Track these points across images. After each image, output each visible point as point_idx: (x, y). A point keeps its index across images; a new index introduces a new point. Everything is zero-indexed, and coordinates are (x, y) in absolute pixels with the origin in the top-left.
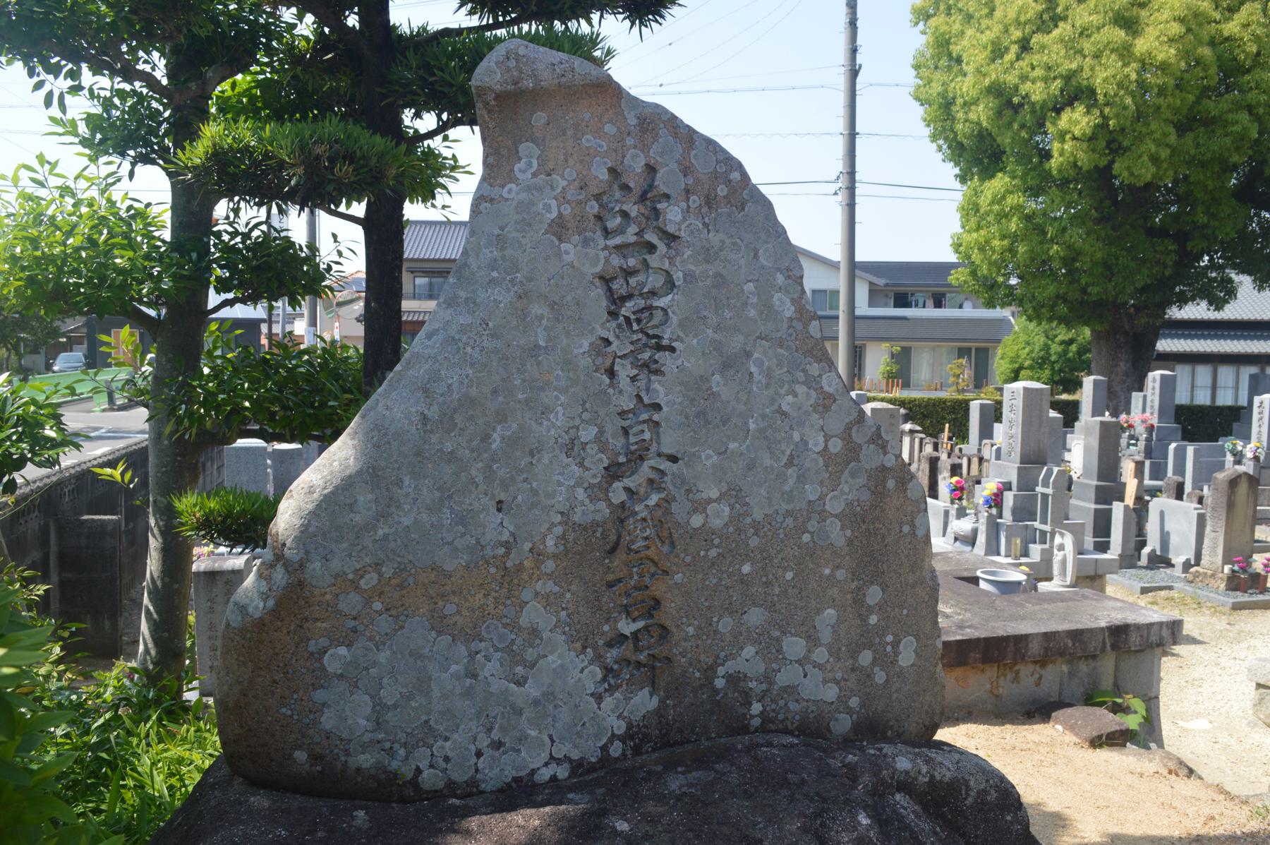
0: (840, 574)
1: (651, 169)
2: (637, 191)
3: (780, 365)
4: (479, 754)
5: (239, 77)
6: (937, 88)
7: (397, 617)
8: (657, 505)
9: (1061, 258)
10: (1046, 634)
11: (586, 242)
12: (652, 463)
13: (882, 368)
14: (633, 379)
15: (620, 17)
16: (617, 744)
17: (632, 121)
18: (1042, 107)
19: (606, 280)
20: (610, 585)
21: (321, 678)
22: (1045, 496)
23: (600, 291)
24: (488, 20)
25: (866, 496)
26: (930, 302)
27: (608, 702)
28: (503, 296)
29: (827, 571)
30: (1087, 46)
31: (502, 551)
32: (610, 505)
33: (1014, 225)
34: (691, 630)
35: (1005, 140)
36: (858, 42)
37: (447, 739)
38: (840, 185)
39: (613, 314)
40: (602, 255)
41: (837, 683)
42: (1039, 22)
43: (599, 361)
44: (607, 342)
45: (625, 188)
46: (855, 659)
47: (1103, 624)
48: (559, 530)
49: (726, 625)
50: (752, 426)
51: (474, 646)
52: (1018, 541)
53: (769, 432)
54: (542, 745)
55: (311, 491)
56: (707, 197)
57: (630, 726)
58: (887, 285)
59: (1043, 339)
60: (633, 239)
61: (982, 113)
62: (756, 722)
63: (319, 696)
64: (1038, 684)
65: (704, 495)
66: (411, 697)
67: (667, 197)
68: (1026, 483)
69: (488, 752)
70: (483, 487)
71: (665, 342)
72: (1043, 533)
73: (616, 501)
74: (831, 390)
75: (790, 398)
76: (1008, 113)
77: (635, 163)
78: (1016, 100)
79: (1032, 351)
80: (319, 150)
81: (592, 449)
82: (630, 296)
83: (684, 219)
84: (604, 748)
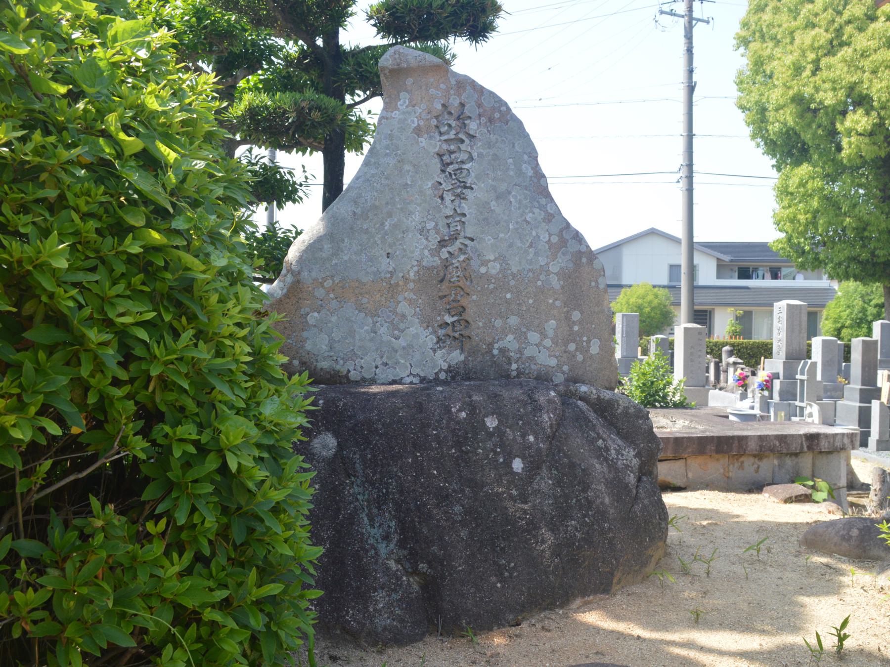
0: (558, 303)
1: (462, 105)
2: (456, 115)
3: (526, 198)
4: (377, 367)
5: (250, 77)
6: (754, 97)
7: (340, 302)
8: (464, 261)
9: (854, 229)
10: (760, 436)
11: (431, 138)
12: (461, 241)
13: (728, 328)
14: (452, 201)
15: (465, 38)
16: (443, 373)
17: (453, 82)
18: (833, 111)
19: (440, 156)
20: (441, 298)
21: (306, 326)
22: (802, 381)
23: (437, 160)
24: (391, 40)
25: (571, 265)
26: (768, 275)
27: (439, 353)
28: (391, 161)
29: (551, 301)
30: (867, 64)
31: (389, 275)
32: (441, 259)
33: (815, 204)
34: (481, 324)
35: (807, 137)
36: (694, 65)
37: (362, 358)
38: (681, 174)
39: (443, 171)
40: (438, 144)
41: (556, 357)
42: (829, 47)
43: (436, 192)
44: (440, 184)
45: (450, 113)
46: (566, 347)
47: (801, 433)
48: (416, 269)
49: (498, 323)
50: (511, 227)
51: (375, 319)
52: (783, 414)
53: (520, 230)
54: (407, 367)
55: (304, 242)
56: (489, 118)
57: (450, 366)
58: (732, 261)
59: (861, 303)
60: (453, 137)
61: (789, 116)
62: (514, 373)
63: (305, 334)
64: (757, 472)
65: (487, 258)
66: (346, 338)
67: (470, 118)
68: (790, 373)
69: (381, 367)
70: (381, 246)
71: (468, 185)
72: (802, 409)
73: (443, 257)
74: (551, 212)
75: (531, 215)
76: (809, 115)
77: (455, 102)
78: (813, 106)
79: (851, 313)
80: (303, 104)
81: (432, 233)
82: (452, 163)
83: (478, 128)
84: (436, 374)
